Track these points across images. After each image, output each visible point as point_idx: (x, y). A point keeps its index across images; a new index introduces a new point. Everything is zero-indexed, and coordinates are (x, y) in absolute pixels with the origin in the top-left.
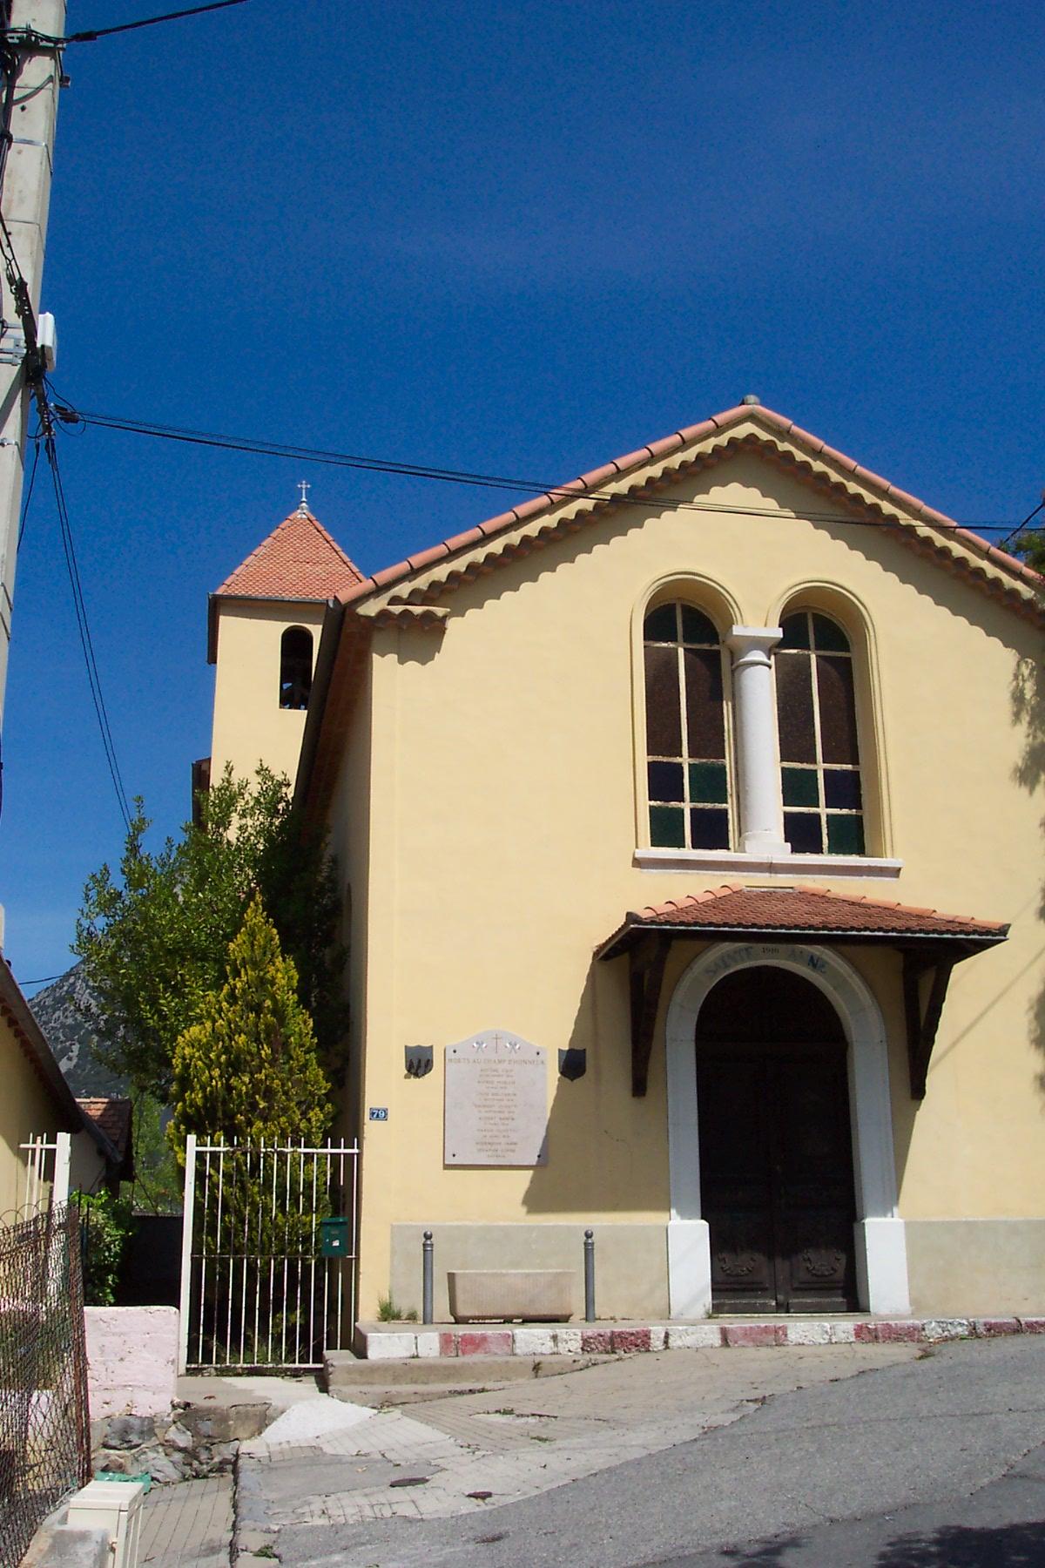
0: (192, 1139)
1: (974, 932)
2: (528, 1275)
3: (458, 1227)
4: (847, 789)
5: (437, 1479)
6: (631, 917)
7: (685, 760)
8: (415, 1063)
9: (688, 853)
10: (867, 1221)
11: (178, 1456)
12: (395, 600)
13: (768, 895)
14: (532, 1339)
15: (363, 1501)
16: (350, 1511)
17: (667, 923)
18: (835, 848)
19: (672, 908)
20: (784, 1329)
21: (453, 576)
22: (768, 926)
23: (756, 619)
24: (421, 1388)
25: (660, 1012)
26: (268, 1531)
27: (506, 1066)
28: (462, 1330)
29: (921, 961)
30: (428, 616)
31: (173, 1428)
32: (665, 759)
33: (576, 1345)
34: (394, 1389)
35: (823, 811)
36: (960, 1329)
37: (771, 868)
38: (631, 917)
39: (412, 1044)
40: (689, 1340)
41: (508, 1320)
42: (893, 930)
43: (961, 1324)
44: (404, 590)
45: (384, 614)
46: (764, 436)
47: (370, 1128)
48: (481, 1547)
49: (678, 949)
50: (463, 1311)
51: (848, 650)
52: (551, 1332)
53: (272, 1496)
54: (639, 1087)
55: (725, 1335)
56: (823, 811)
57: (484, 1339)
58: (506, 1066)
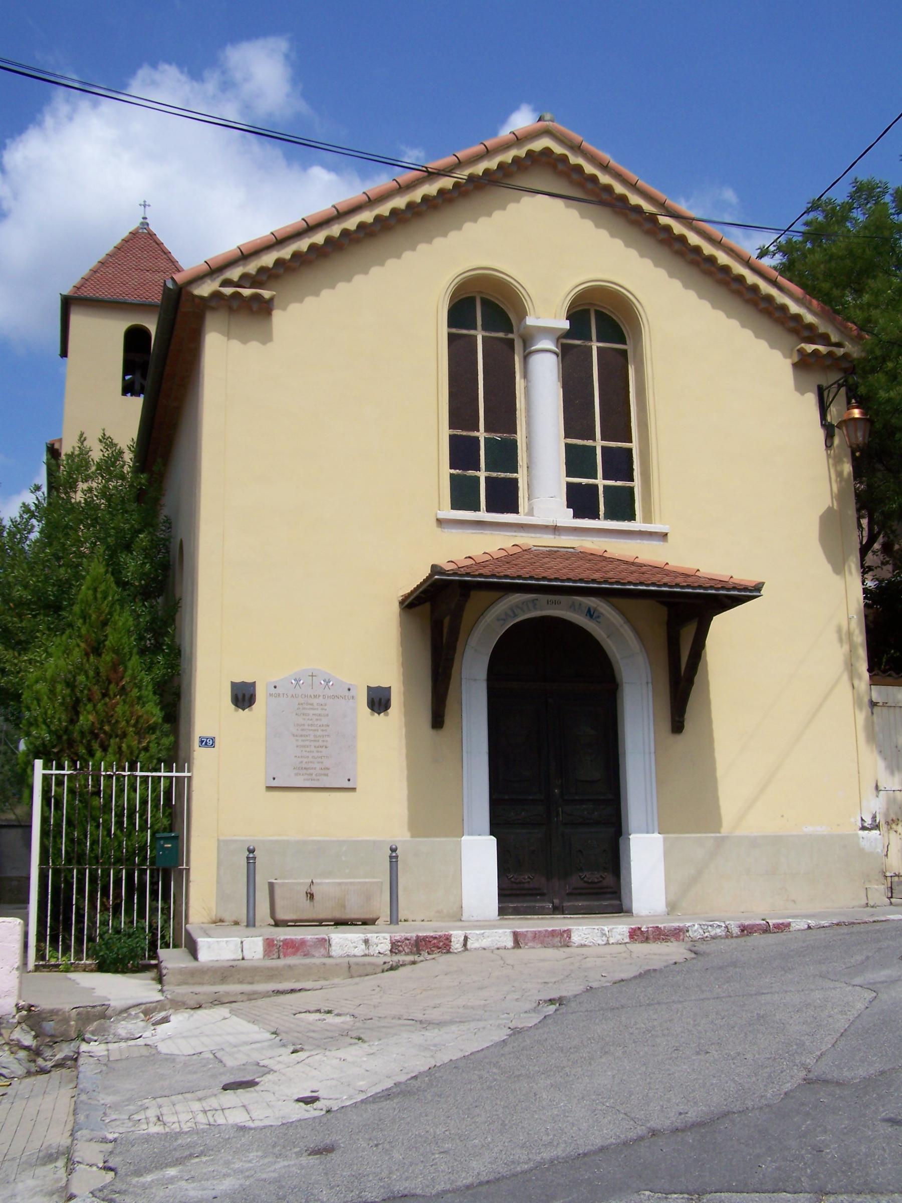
0: (39, 763)
1: (734, 588)
2: (340, 884)
3: (277, 841)
4: (620, 464)
5: (266, 1081)
6: (436, 569)
7: (482, 434)
8: (240, 697)
9: (483, 515)
10: (631, 837)
11: (22, 1054)
12: (227, 283)
13: (552, 553)
14: (346, 942)
15: (196, 1106)
16: (184, 1117)
17: (468, 574)
18: (609, 516)
19: (470, 562)
20: (568, 932)
21: (279, 262)
22: (556, 579)
23: (547, 313)
24: (246, 988)
25: (458, 655)
26: (104, 1140)
27: (320, 700)
28: (284, 934)
29: (686, 612)
30: (257, 297)
31: (18, 1028)
32: (464, 433)
33: (386, 947)
34: (222, 988)
35: (600, 482)
36: (718, 930)
37: (556, 529)
38: (436, 569)
39: (238, 680)
40: (485, 943)
41: (320, 923)
42: (665, 585)
43: (719, 926)
44: (235, 274)
45: (216, 295)
46: (558, 149)
47: (199, 754)
48: (314, 1160)
49: (477, 598)
50: (281, 915)
51: (625, 343)
52: (362, 936)
53: (109, 1100)
54: (438, 721)
55: (518, 940)
56: (600, 482)
57: (303, 943)
58: (320, 700)
